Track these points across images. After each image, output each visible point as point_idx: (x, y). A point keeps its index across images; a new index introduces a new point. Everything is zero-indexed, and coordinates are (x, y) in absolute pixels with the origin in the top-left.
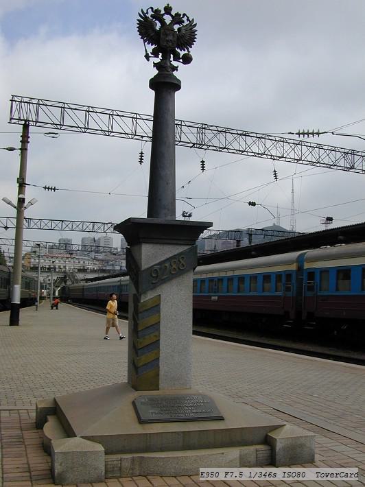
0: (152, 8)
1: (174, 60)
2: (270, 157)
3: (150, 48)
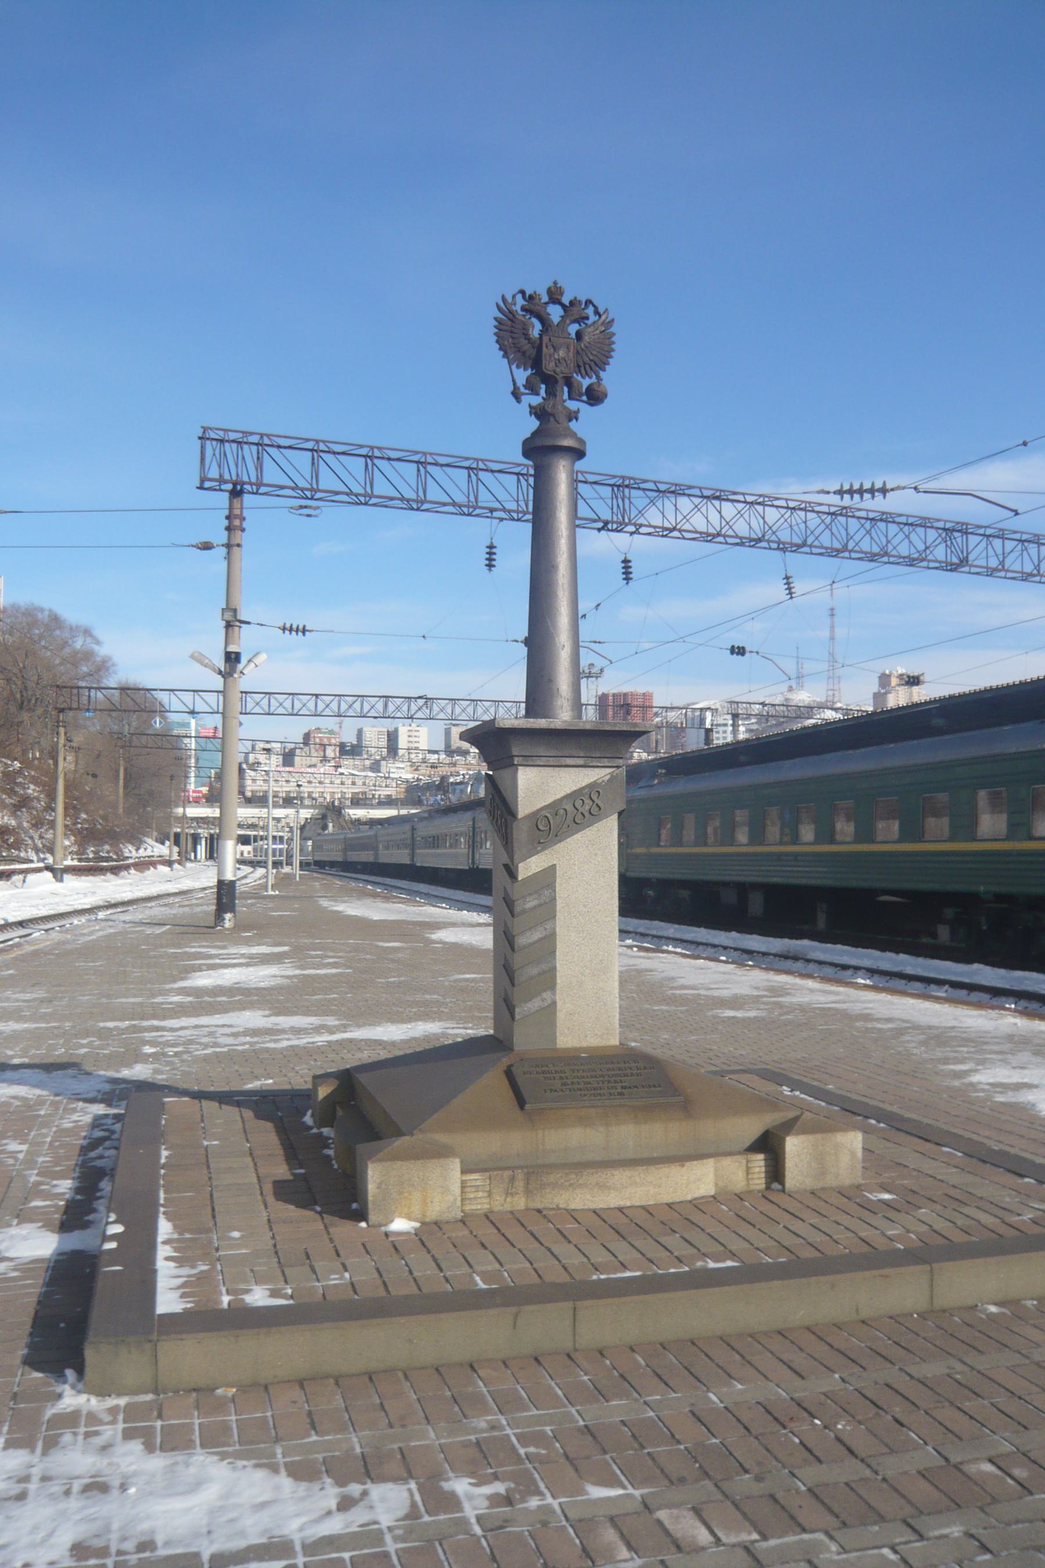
0: (523, 292)
1: (570, 398)
2: (774, 546)
3: (522, 375)
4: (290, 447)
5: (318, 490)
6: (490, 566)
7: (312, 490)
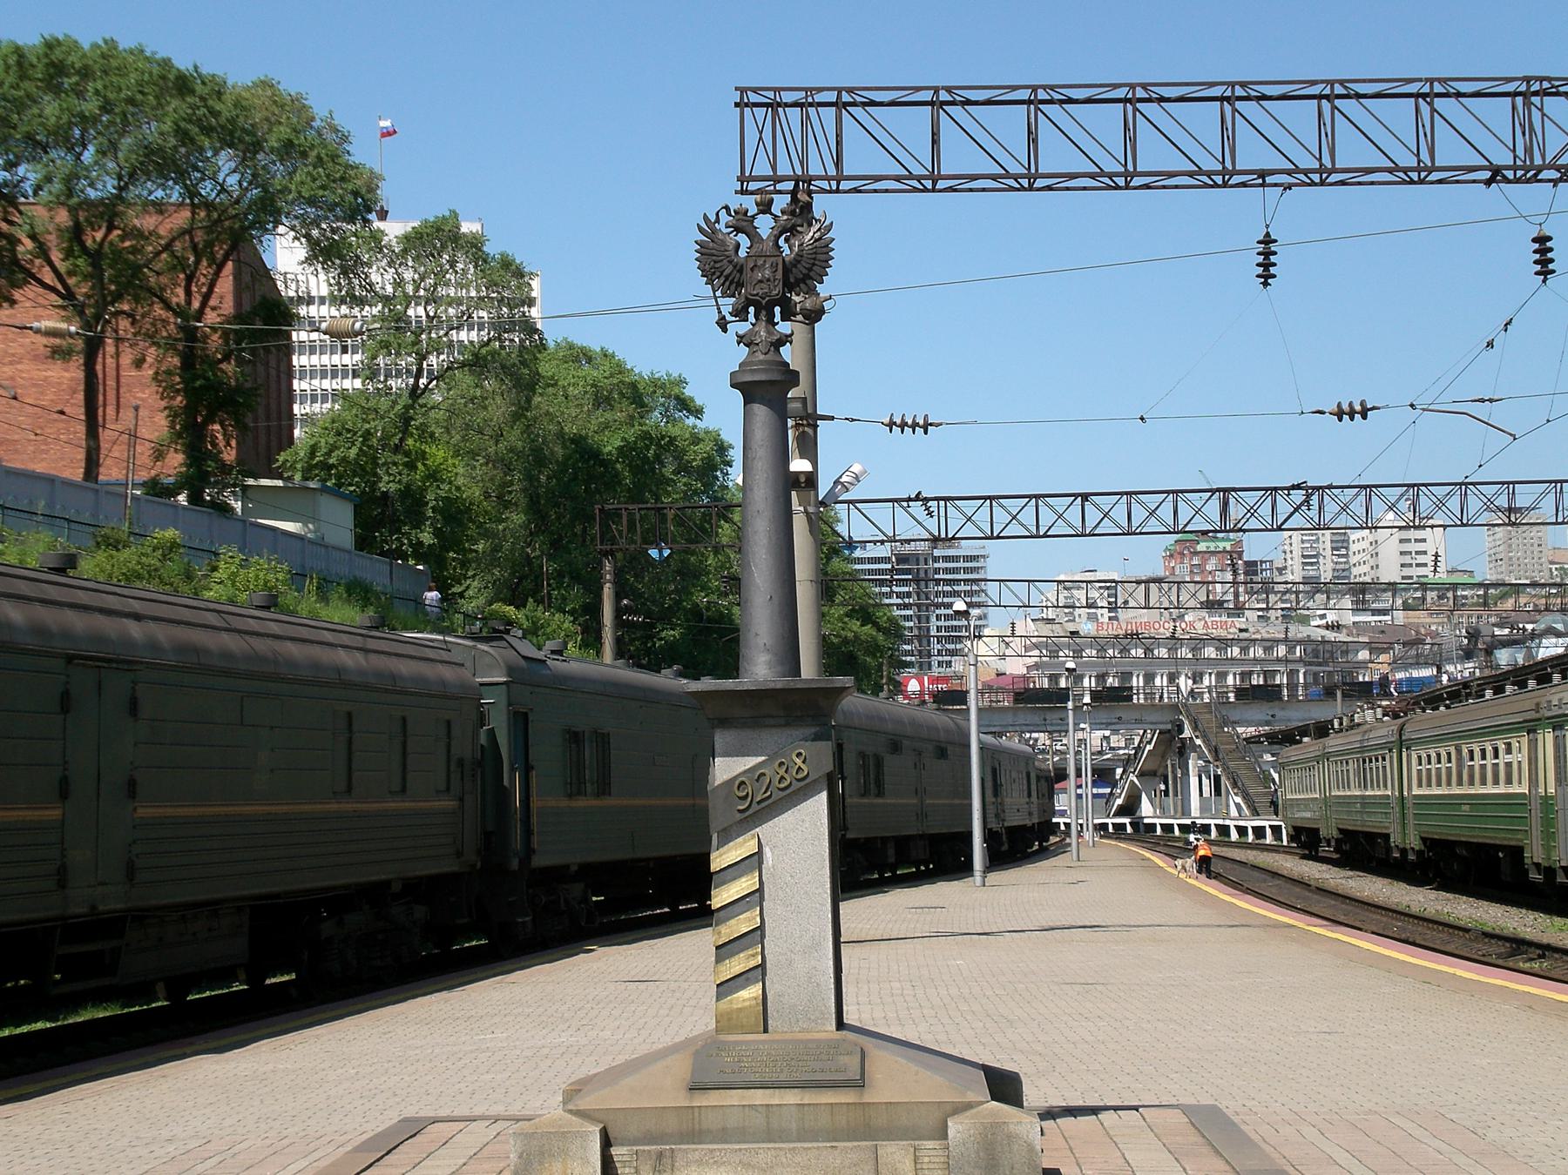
0: (727, 208)
3: (728, 304)
6: (1266, 278)
7: (1028, 176)
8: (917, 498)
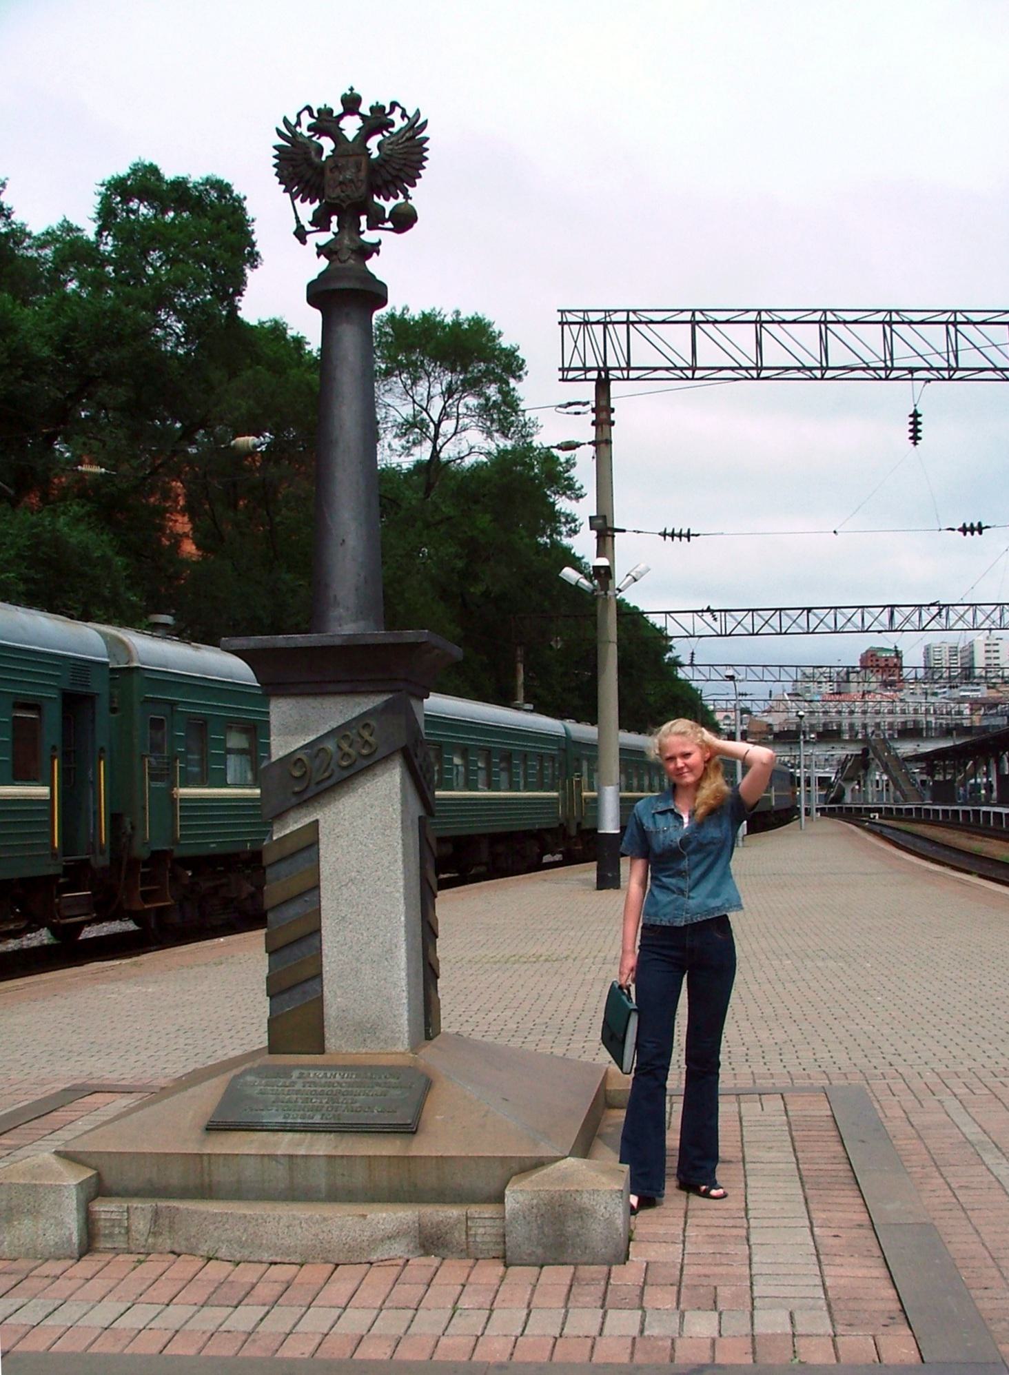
0: (308, 108)
1: (370, 228)
3: (307, 210)
4: (727, 322)
5: (762, 368)
6: (915, 439)
8: (708, 610)
